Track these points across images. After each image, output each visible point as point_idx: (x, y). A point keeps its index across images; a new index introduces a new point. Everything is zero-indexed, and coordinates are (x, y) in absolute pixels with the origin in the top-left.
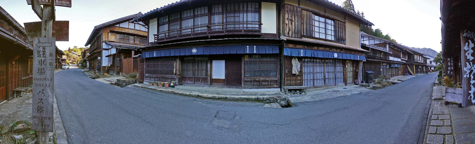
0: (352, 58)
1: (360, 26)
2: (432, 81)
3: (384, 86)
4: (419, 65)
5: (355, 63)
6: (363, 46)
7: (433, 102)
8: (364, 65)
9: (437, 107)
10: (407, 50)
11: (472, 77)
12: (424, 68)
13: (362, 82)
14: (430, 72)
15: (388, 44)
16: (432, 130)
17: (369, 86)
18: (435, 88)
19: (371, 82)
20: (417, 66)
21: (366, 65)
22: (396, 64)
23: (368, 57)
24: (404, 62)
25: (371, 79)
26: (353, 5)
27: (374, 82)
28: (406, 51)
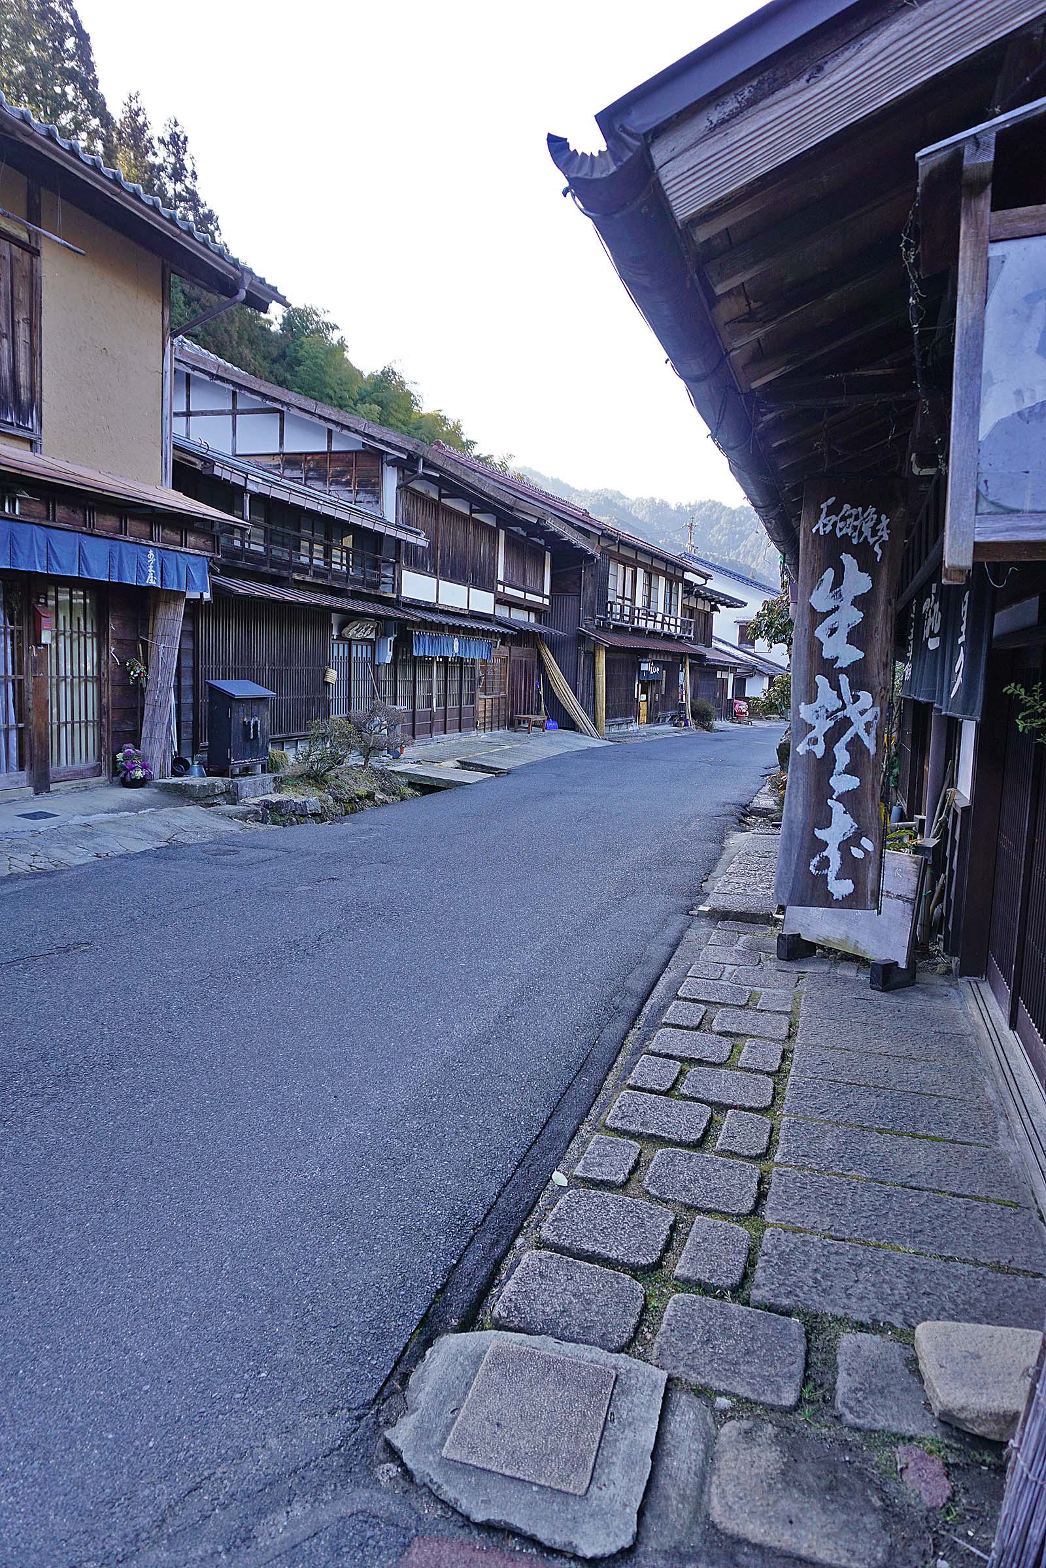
0: (99, 573)
1: (166, 299)
2: (731, 792)
3: (353, 805)
4: (644, 653)
5: (124, 608)
6: (191, 474)
7: (700, 931)
8: (191, 634)
9: (717, 961)
10: (553, 525)
11: (843, 757)
12: (685, 677)
13: (180, 766)
14: (736, 717)
15: (396, 463)
16: (648, 1071)
17: (232, 796)
18: (738, 840)
19: (246, 771)
20: (625, 662)
21: (209, 631)
22: (455, 630)
23: (232, 564)
24: (519, 616)
25: (251, 742)
26: (83, 38)
27: (270, 767)
28: (538, 529)
